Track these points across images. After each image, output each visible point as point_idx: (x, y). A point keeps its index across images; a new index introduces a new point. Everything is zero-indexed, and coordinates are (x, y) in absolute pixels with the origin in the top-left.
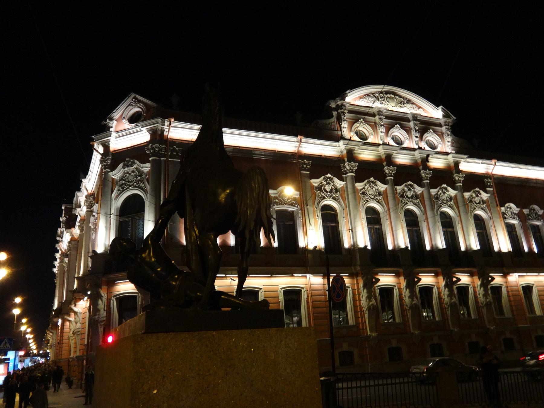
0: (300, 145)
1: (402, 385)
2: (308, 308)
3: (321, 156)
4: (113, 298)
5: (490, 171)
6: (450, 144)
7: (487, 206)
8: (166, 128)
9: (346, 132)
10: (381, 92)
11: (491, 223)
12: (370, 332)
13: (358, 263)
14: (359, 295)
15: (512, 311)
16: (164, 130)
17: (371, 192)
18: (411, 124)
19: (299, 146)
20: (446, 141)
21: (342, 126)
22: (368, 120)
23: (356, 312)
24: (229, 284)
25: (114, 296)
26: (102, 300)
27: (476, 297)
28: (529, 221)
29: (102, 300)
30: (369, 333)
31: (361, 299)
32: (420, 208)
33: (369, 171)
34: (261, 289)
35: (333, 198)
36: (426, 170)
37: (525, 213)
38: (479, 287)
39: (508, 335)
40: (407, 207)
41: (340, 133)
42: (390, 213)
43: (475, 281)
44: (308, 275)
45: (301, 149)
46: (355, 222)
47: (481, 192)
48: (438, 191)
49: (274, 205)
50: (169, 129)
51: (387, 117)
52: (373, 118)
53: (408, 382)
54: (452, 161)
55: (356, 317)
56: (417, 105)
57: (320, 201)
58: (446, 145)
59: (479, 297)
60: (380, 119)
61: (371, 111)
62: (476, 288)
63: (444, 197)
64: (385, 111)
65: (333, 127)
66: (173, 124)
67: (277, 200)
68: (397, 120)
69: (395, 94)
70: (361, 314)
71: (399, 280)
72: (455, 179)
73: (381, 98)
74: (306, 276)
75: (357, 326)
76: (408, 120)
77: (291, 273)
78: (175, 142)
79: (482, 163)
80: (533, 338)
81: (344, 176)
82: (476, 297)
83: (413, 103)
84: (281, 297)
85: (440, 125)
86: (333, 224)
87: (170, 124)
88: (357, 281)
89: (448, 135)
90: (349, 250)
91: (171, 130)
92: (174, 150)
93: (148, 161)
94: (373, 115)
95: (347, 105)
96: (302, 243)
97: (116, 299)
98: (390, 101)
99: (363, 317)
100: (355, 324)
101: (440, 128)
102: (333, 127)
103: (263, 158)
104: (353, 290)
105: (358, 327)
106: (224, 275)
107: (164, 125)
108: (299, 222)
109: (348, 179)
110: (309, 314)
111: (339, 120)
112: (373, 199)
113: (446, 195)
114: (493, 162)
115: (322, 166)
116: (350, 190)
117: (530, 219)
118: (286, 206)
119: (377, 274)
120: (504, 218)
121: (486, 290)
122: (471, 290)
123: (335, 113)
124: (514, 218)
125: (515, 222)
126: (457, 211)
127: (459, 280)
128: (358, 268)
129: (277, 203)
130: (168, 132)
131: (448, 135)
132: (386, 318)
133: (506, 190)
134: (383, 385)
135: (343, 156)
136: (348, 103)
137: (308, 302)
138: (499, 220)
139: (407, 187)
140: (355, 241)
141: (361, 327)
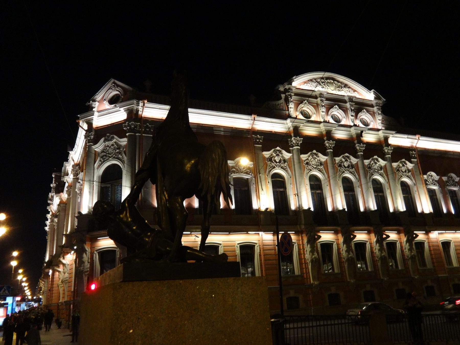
0: (253, 122)
1: (340, 326)
2: (261, 260)
3: (272, 132)
4: (95, 252)
5: (414, 145)
6: (380, 121)
7: (412, 174)
8: (140, 108)
9: (292, 111)
10: (322, 78)
11: (415, 189)
12: (313, 281)
13: (303, 222)
14: (304, 249)
15: (433, 263)
16: (139, 110)
17: (314, 162)
18: (348, 105)
19: (253, 124)
20: (377, 119)
21: (290, 106)
22: (311, 102)
23: (301, 263)
24: (194, 240)
25: (96, 251)
26: (86, 254)
27: (402, 251)
28: (447, 187)
29: (86, 254)
30: (312, 282)
31: (306, 253)
32: (355, 176)
33: (312, 144)
34: (220, 244)
35: (282, 168)
36: (360, 144)
37: (444, 180)
38: (405, 243)
39: (430, 283)
40: (344, 175)
41: (287, 112)
42: (329, 180)
43: (402, 237)
44: (260, 233)
45: (254, 126)
46: (300, 188)
47: (407, 162)
48: (371, 162)
49: (231, 174)
50: (143, 109)
51: (327, 99)
52: (316, 100)
53: (345, 323)
54: (382, 136)
55: (301, 268)
56: (352, 89)
57: (271, 170)
58: (377, 122)
59: (405, 251)
60: (321, 100)
61: (314, 94)
62: (403, 244)
63: (376, 167)
64: (325, 93)
65: (281, 107)
66: (146, 105)
67: (234, 169)
68: (336, 102)
69: (334, 79)
70: (305, 266)
71: (338, 237)
72: (385, 152)
73: (322, 83)
74: (259, 234)
75: (302, 276)
76: (345, 102)
77: (246, 231)
78: (148, 120)
79: (407, 138)
80: (451, 286)
81: (291, 149)
82: (402, 251)
83: (349, 87)
84: (238, 251)
85: (372, 106)
86: (282, 190)
87: (144, 105)
88: (302, 237)
89: (379, 114)
90: (295, 211)
91: (144, 110)
92: (147, 127)
93: (125, 137)
94: (316, 97)
95: (294, 89)
96: (255, 206)
97: (98, 253)
98: (330, 85)
99: (307, 268)
100: (300, 274)
101: (372, 108)
102: (281, 107)
103: (222, 133)
104: (299, 245)
105: (303, 276)
106: (189, 233)
107: (139, 106)
108: (253, 188)
109: (294, 152)
110: (261, 266)
111: (287, 101)
112: (316, 168)
113: (377, 165)
114: (417, 137)
115: (272, 140)
116: (296, 161)
117: (448, 185)
118: (242, 174)
119: (319, 232)
120: (426, 184)
121: (411, 245)
122: (398, 245)
123: (283, 96)
124: (435, 184)
125: (435, 188)
126: (386, 178)
127: (388, 237)
128: (303, 227)
129: (234, 172)
130: (142, 111)
131: (379, 114)
132: (326, 269)
133: (428, 161)
134: (324, 325)
135: (290, 132)
136: (294, 87)
137: (260, 255)
138: (422, 186)
139: (345, 159)
140: (300, 203)
141: (305, 277)
